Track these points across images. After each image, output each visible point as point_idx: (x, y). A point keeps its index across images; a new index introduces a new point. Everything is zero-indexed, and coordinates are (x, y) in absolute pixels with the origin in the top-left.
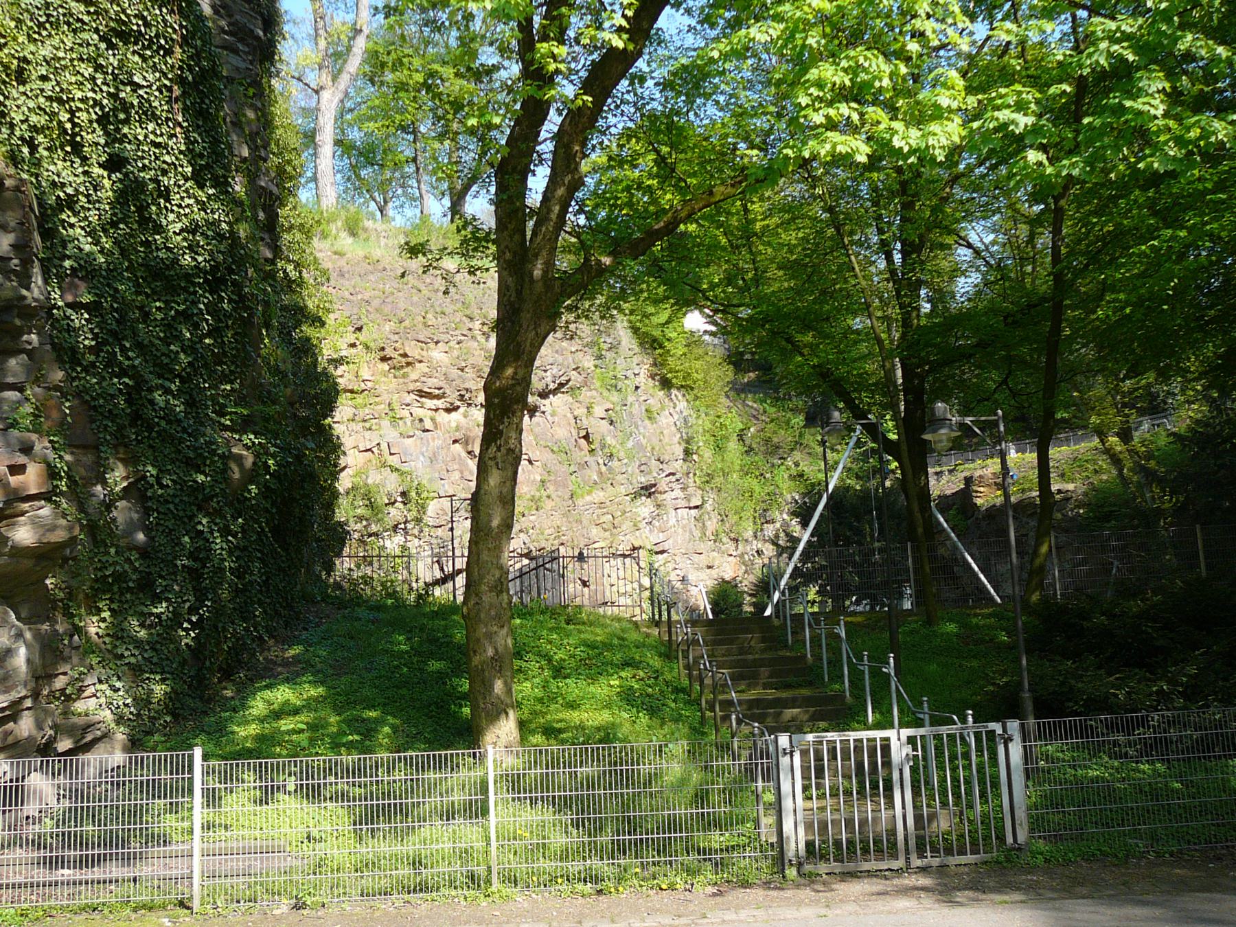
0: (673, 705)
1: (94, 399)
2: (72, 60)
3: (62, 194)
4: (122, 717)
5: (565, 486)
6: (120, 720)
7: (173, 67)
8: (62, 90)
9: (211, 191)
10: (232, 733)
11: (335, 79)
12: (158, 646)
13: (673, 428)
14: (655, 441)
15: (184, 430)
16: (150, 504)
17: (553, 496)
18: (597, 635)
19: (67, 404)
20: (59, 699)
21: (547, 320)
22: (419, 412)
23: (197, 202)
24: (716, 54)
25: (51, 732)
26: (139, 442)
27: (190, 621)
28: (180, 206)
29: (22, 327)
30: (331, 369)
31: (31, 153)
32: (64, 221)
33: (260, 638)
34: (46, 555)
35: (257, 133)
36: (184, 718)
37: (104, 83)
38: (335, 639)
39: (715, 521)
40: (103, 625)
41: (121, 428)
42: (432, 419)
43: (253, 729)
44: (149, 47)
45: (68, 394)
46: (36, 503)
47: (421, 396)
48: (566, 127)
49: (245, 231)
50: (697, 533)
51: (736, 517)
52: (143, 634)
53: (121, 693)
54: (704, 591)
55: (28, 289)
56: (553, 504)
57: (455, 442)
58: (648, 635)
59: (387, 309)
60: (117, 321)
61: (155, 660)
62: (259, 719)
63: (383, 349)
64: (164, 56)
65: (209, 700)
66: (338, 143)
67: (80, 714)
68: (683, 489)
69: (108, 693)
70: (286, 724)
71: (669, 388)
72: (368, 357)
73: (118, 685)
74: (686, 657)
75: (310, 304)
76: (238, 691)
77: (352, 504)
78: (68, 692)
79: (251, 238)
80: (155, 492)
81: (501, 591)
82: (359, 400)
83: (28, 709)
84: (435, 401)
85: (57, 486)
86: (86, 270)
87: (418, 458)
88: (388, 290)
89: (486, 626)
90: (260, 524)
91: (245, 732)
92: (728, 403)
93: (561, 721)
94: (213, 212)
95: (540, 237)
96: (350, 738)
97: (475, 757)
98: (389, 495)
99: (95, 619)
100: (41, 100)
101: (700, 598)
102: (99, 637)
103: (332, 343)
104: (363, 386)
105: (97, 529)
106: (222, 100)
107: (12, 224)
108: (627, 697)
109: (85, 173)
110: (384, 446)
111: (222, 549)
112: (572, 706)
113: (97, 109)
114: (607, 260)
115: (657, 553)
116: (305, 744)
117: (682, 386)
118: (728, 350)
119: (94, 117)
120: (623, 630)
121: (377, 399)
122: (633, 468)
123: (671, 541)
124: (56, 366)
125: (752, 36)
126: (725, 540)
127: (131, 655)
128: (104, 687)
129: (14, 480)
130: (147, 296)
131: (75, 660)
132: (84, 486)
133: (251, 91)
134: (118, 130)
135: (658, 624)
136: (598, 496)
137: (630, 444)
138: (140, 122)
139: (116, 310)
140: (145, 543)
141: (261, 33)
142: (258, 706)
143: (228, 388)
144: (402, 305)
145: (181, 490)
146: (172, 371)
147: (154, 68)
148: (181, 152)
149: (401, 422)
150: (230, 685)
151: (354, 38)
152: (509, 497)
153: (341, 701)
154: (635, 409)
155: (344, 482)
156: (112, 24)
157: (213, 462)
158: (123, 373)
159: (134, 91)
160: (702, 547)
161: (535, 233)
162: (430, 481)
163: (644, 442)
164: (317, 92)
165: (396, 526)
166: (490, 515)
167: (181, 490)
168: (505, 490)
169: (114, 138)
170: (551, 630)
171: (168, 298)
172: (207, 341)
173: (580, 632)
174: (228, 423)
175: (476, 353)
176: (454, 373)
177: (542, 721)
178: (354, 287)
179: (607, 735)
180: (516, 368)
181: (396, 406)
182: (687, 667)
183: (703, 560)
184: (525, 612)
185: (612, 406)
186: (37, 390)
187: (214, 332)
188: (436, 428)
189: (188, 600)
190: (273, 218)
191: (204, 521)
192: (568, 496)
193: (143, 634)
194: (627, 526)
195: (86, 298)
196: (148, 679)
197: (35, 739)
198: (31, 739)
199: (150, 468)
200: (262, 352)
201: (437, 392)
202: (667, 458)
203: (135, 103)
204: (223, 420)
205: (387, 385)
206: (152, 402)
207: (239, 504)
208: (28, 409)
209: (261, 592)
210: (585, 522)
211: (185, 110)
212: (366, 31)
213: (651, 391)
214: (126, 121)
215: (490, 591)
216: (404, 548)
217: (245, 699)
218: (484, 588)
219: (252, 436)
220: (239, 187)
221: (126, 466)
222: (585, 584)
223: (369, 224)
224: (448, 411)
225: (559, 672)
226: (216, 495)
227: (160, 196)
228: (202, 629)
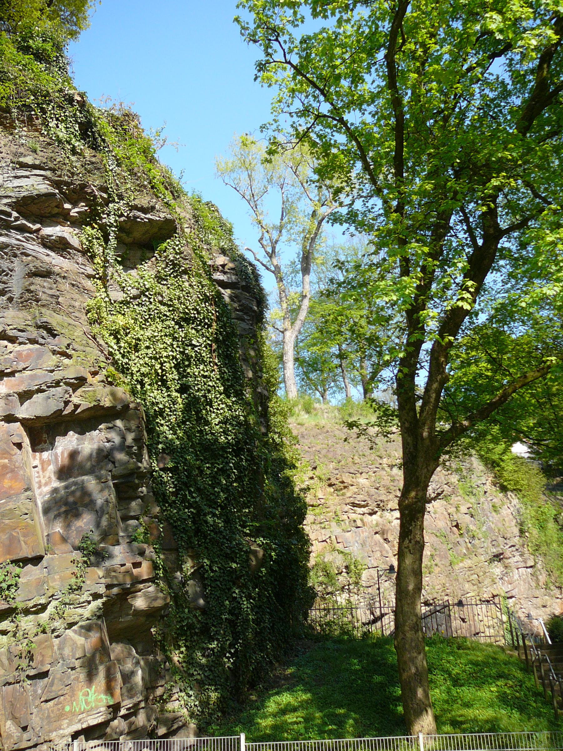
0: (534, 705)
1: (175, 522)
2: (161, 336)
3: (157, 408)
4: (193, 713)
5: (446, 558)
6: (192, 715)
7: (212, 333)
8: (156, 353)
9: (234, 399)
10: (258, 723)
11: (293, 323)
12: (213, 669)
13: (511, 517)
14: (500, 525)
15: (224, 537)
16: (206, 582)
17: (439, 565)
18: (478, 656)
19: (161, 526)
20: (159, 702)
21: (433, 462)
22: (353, 516)
23: (227, 406)
24: (523, 304)
25: (155, 723)
26: (200, 545)
27: (230, 653)
28: (218, 409)
29: (138, 484)
30: (302, 495)
31: (142, 388)
32: (158, 423)
33: (271, 662)
34: (152, 615)
35: (256, 363)
36: (229, 714)
37: (177, 347)
38: (315, 662)
39: (544, 575)
40: (181, 656)
41: (190, 538)
42: (362, 520)
43: (269, 721)
44: (200, 325)
45: (162, 519)
46: (147, 584)
47: (354, 506)
48: (436, 348)
49: (253, 420)
50: (533, 584)
51: (558, 573)
52: (204, 661)
53: (193, 698)
54: (542, 622)
55: (141, 462)
56: (439, 569)
57: (376, 533)
58: (511, 656)
59: (330, 455)
60: (187, 476)
61: (211, 677)
62: (273, 715)
63: (329, 479)
64: (207, 328)
65: (243, 702)
66: (296, 360)
67: (170, 712)
68: (521, 555)
69: (185, 698)
70: (290, 718)
71: (506, 491)
72: (321, 484)
73: (191, 693)
74: (539, 670)
75: (287, 456)
76: (259, 697)
77: (316, 575)
78: (164, 697)
79: (256, 423)
80: (209, 575)
81: (418, 631)
82: (317, 511)
83: (143, 708)
84: (362, 509)
85: (158, 574)
86: (170, 449)
87: (354, 544)
88: (330, 444)
89: (410, 653)
90: (268, 591)
91: (265, 723)
92: (544, 498)
93: (461, 716)
94: (235, 411)
95: (425, 413)
96: (330, 727)
97: (408, 741)
98: (338, 568)
99: (177, 652)
100: (147, 359)
101: (540, 626)
102: (180, 663)
103: (300, 478)
104: (319, 502)
105: (179, 598)
106: (237, 348)
107: (134, 428)
108: (503, 699)
109: (169, 396)
110: (333, 538)
111: (247, 608)
112: (467, 705)
113: (174, 361)
114: (466, 423)
115: (508, 598)
116: (303, 731)
117: (514, 490)
118: (542, 464)
119: (173, 365)
120: (494, 653)
121: (327, 510)
122: (488, 544)
123: (516, 590)
124: (155, 504)
125: (544, 292)
126: (552, 588)
127: (198, 674)
128: (183, 694)
129: (135, 571)
130: (202, 461)
131: (167, 678)
132: (171, 572)
133: (252, 341)
134: (185, 371)
135: (517, 648)
136: (468, 563)
137: (484, 529)
138: (196, 365)
139: (186, 471)
140: (205, 605)
141: (256, 308)
142: (272, 706)
143: (247, 511)
144: (339, 452)
145: (224, 573)
146: (216, 503)
147: (203, 335)
148: (217, 379)
149: (342, 523)
150: (254, 693)
151: (302, 300)
152: (418, 571)
153: (322, 702)
154: (486, 506)
155: (312, 562)
156: (181, 315)
157: (241, 556)
158: (190, 506)
159: (193, 349)
160: (537, 593)
161: (422, 411)
162: (363, 558)
163: (493, 526)
164: (283, 332)
165: (343, 587)
166: (407, 582)
167: (224, 573)
168: (416, 567)
169: (182, 375)
170: (449, 654)
171: (213, 461)
172: (235, 484)
173: (467, 654)
174: (248, 531)
175: (385, 478)
176: (373, 491)
177: (449, 715)
178: (310, 443)
179: (493, 726)
180: (417, 492)
181: (339, 513)
182: (540, 677)
183: (539, 602)
184: (431, 643)
185: (471, 506)
186: (146, 518)
187: (239, 479)
188: (364, 525)
189: (229, 640)
190: (265, 408)
191: (237, 591)
192: (448, 564)
193: (204, 661)
194: (487, 581)
195: (170, 465)
196: (208, 689)
197: (146, 727)
198: (144, 727)
199: (206, 561)
200: (265, 488)
201: (363, 503)
202: (508, 536)
203: (193, 355)
204: (245, 530)
205: (334, 501)
206: (206, 522)
207: (256, 580)
208: (141, 530)
209: (270, 633)
210: (461, 580)
211: (219, 356)
212: (309, 296)
213: (495, 494)
214: (189, 366)
215: (411, 630)
216: (349, 601)
217: (263, 701)
218: (407, 628)
219: (262, 539)
220: (248, 395)
221: (193, 560)
222: (463, 620)
223: (317, 405)
224: (371, 514)
225: (456, 682)
226: (243, 575)
227: (207, 405)
228: (237, 657)
